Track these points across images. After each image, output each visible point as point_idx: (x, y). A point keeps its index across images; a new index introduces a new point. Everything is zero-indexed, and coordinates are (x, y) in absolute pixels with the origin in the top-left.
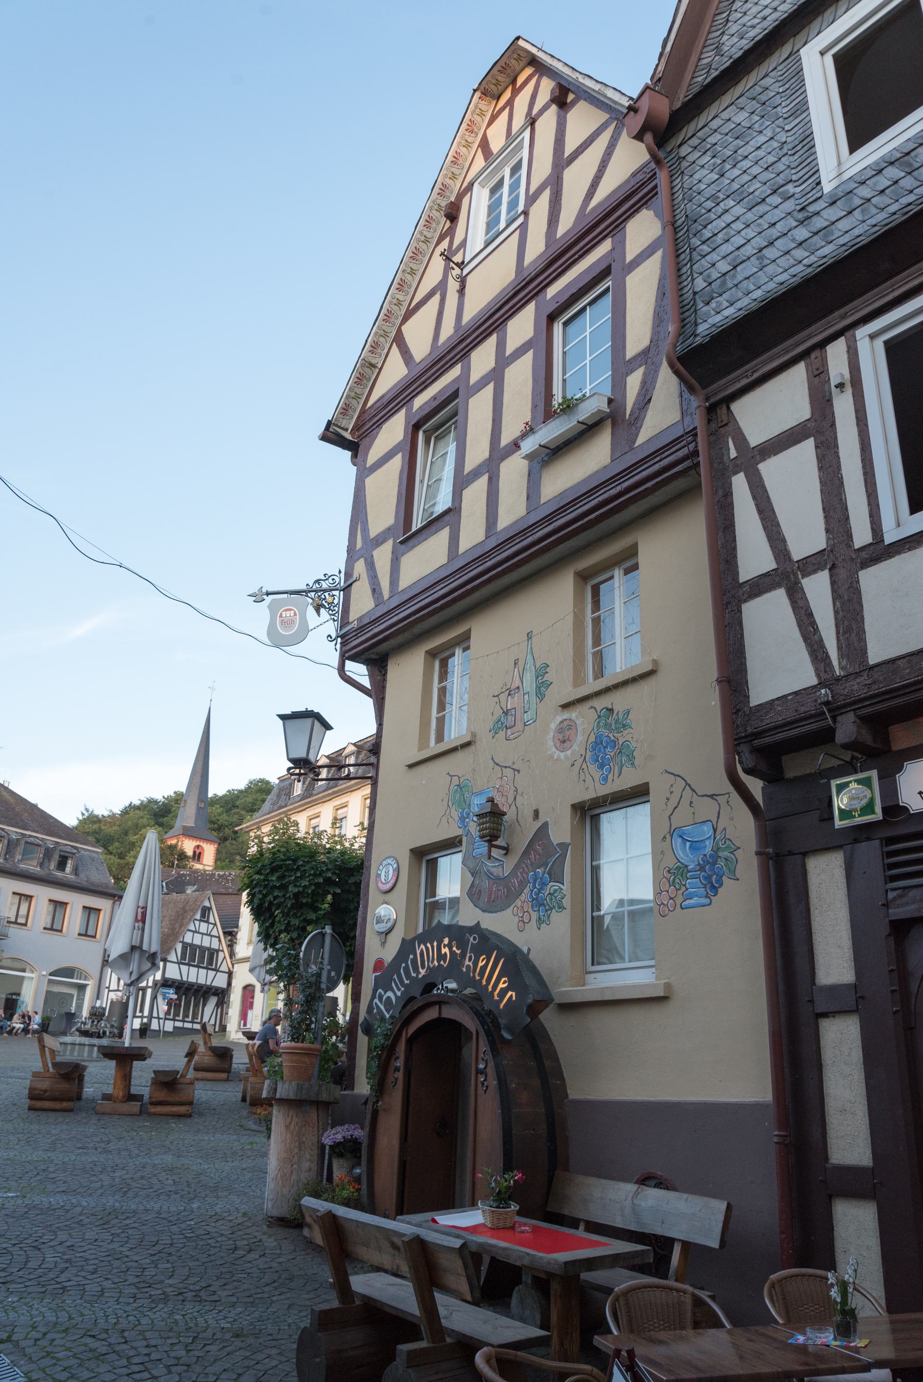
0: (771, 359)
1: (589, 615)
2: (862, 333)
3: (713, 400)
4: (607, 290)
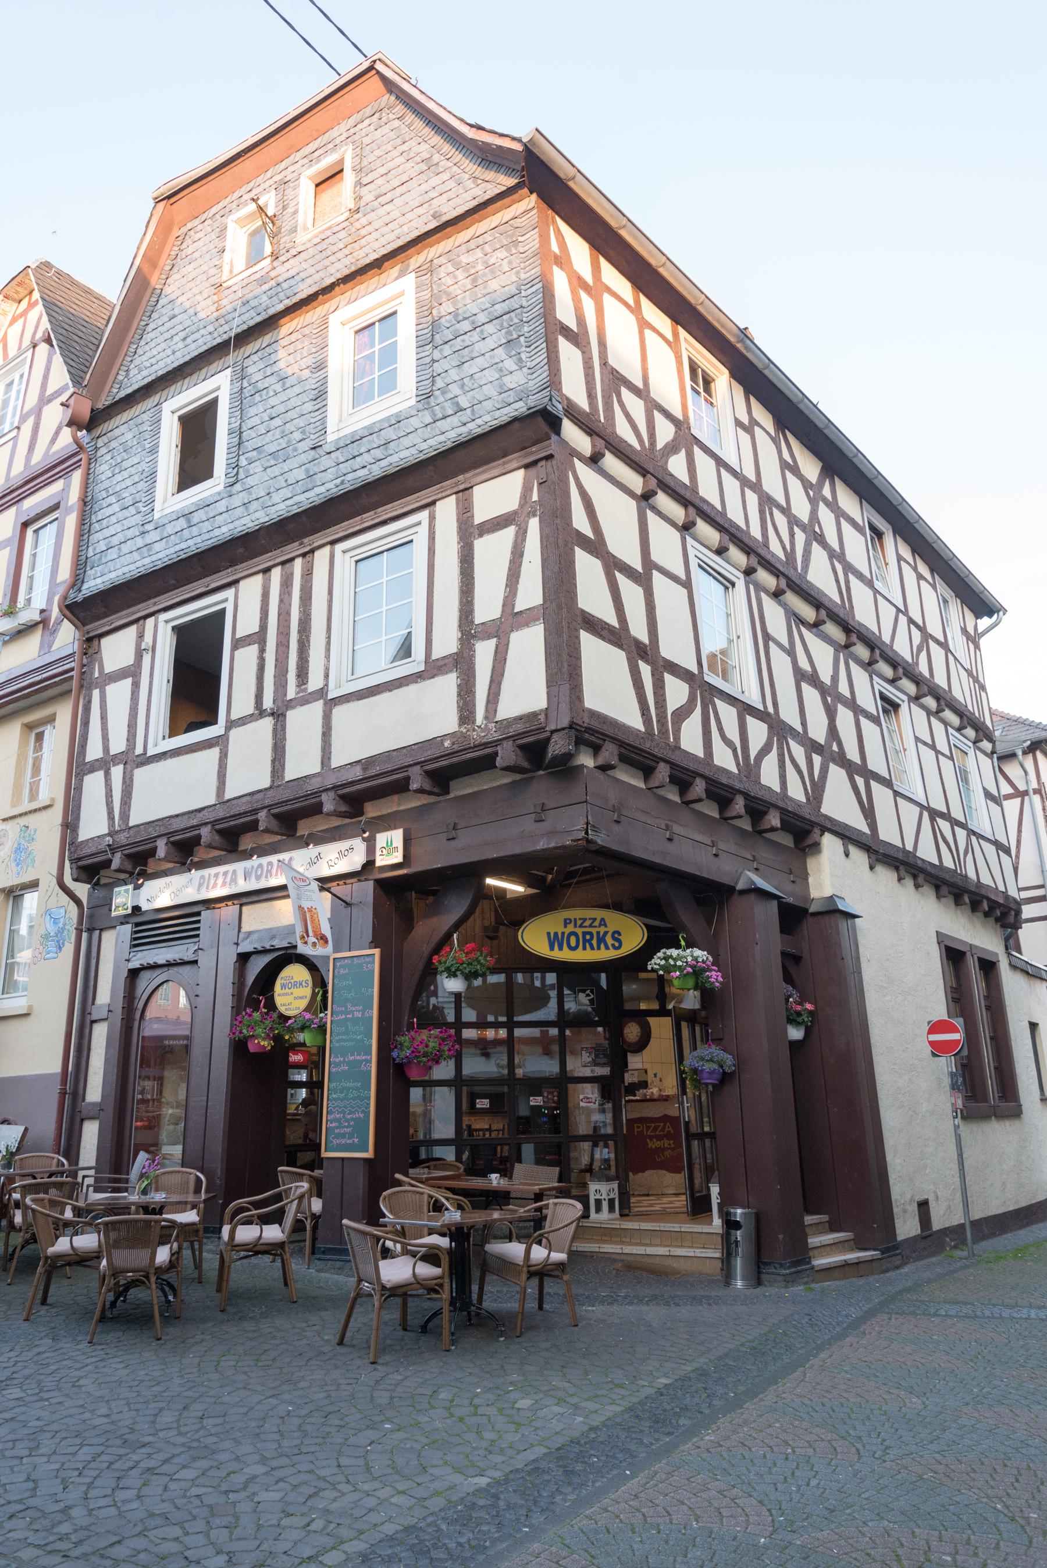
0: (120, 618)
1: (31, 755)
2: (163, 617)
3: (91, 634)
4: (56, 519)
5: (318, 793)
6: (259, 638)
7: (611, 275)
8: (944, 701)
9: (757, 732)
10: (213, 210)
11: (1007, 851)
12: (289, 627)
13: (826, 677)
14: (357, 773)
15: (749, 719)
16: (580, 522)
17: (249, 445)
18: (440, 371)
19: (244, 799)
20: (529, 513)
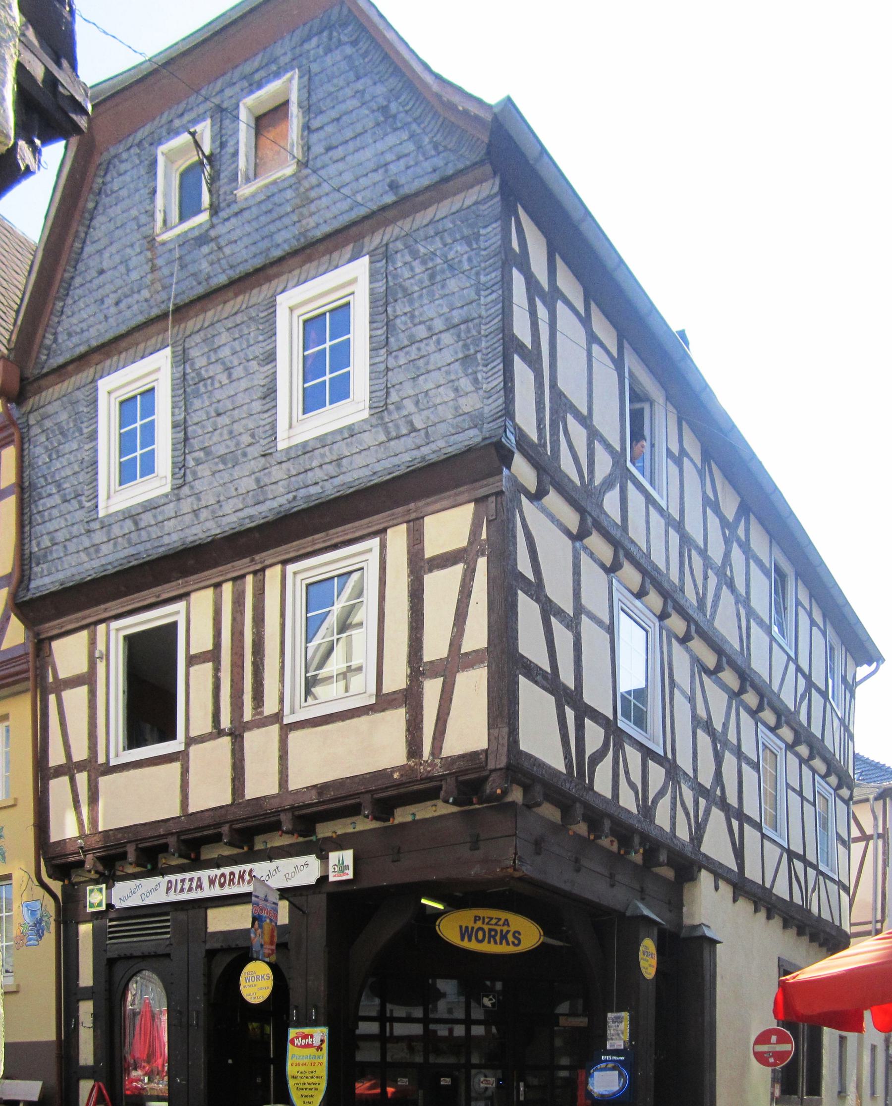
0: (71, 622)
2: (115, 625)
5: (278, 812)
6: (214, 655)
7: (566, 282)
8: (817, 748)
9: (657, 774)
10: (140, 135)
11: (847, 889)
12: (243, 648)
13: (718, 726)
14: (313, 798)
15: (651, 763)
16: (524, 566)
17: (195, 443)
18: (395, 381)
19: (207, 814)
20: (477, 552)
